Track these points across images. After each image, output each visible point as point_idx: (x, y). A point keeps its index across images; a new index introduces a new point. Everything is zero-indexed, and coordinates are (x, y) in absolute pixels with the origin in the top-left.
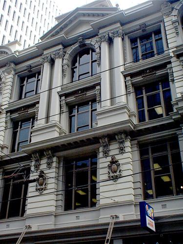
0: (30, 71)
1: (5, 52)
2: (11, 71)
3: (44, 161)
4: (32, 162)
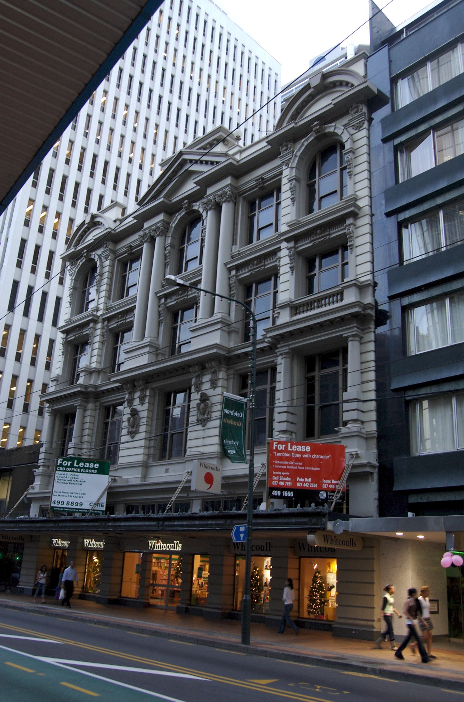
0: (131, 254)
1: (347, 84)
2: (362, 123)
3: (207, 378)
4: (277, 356)
